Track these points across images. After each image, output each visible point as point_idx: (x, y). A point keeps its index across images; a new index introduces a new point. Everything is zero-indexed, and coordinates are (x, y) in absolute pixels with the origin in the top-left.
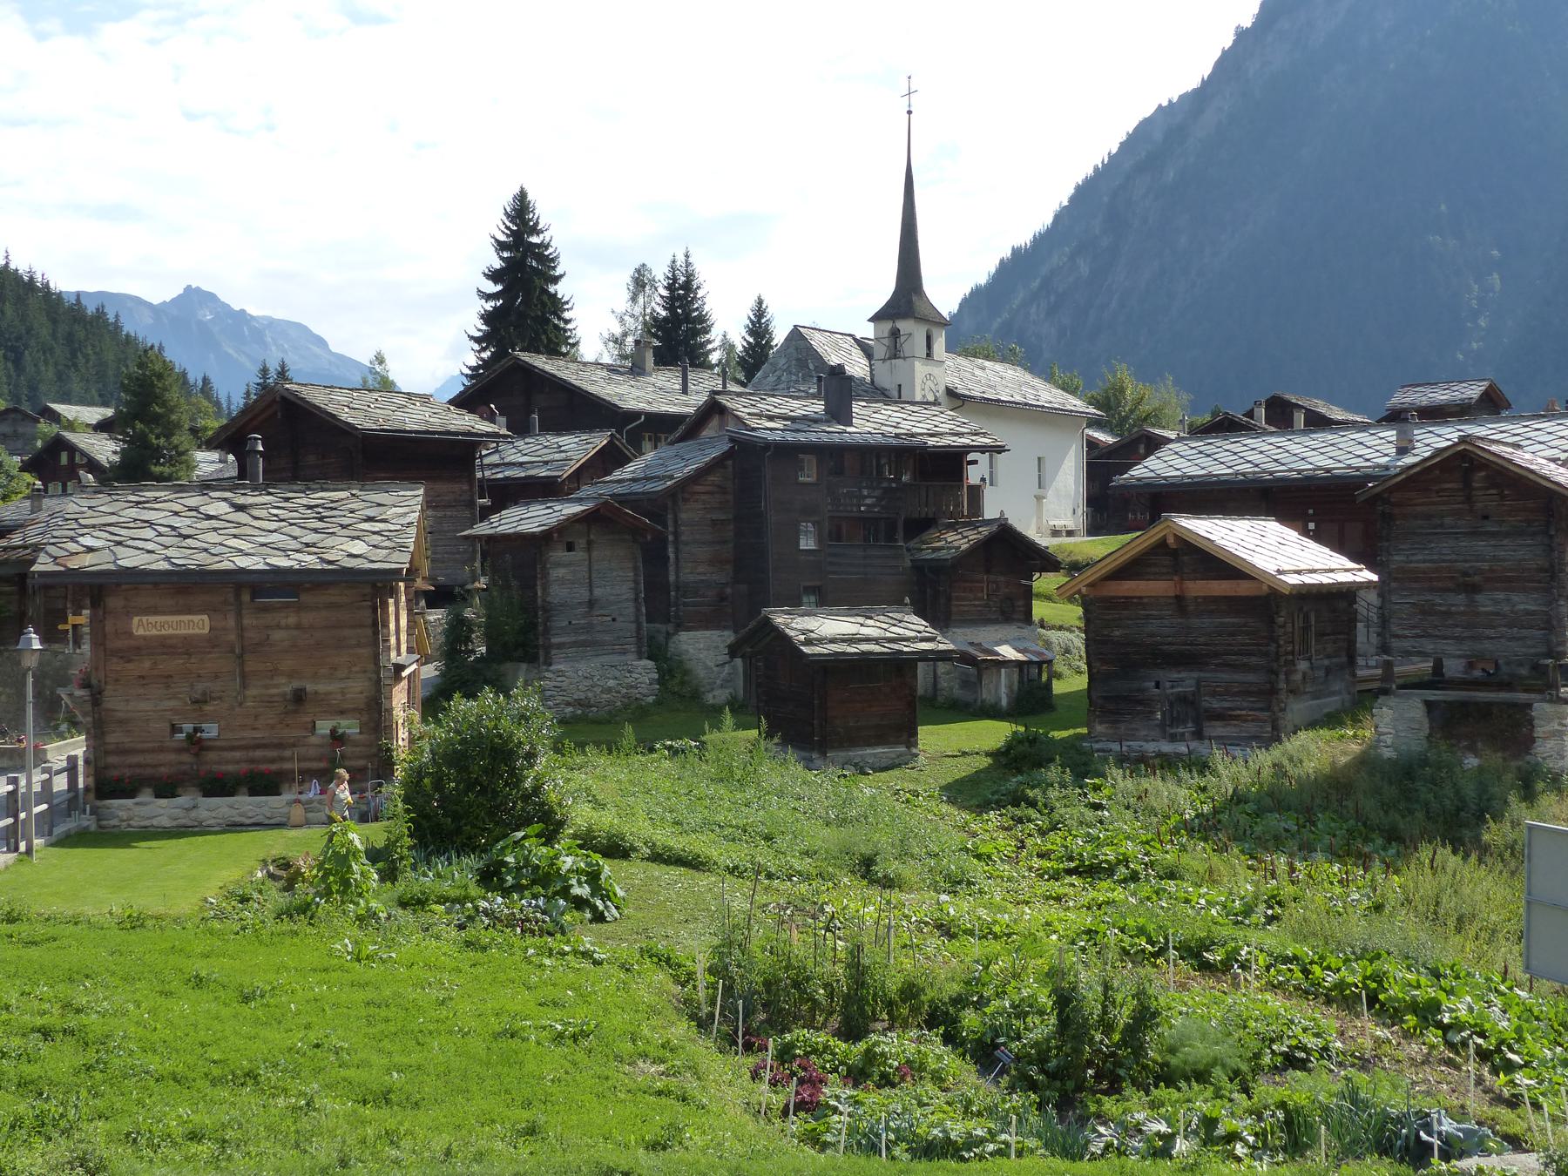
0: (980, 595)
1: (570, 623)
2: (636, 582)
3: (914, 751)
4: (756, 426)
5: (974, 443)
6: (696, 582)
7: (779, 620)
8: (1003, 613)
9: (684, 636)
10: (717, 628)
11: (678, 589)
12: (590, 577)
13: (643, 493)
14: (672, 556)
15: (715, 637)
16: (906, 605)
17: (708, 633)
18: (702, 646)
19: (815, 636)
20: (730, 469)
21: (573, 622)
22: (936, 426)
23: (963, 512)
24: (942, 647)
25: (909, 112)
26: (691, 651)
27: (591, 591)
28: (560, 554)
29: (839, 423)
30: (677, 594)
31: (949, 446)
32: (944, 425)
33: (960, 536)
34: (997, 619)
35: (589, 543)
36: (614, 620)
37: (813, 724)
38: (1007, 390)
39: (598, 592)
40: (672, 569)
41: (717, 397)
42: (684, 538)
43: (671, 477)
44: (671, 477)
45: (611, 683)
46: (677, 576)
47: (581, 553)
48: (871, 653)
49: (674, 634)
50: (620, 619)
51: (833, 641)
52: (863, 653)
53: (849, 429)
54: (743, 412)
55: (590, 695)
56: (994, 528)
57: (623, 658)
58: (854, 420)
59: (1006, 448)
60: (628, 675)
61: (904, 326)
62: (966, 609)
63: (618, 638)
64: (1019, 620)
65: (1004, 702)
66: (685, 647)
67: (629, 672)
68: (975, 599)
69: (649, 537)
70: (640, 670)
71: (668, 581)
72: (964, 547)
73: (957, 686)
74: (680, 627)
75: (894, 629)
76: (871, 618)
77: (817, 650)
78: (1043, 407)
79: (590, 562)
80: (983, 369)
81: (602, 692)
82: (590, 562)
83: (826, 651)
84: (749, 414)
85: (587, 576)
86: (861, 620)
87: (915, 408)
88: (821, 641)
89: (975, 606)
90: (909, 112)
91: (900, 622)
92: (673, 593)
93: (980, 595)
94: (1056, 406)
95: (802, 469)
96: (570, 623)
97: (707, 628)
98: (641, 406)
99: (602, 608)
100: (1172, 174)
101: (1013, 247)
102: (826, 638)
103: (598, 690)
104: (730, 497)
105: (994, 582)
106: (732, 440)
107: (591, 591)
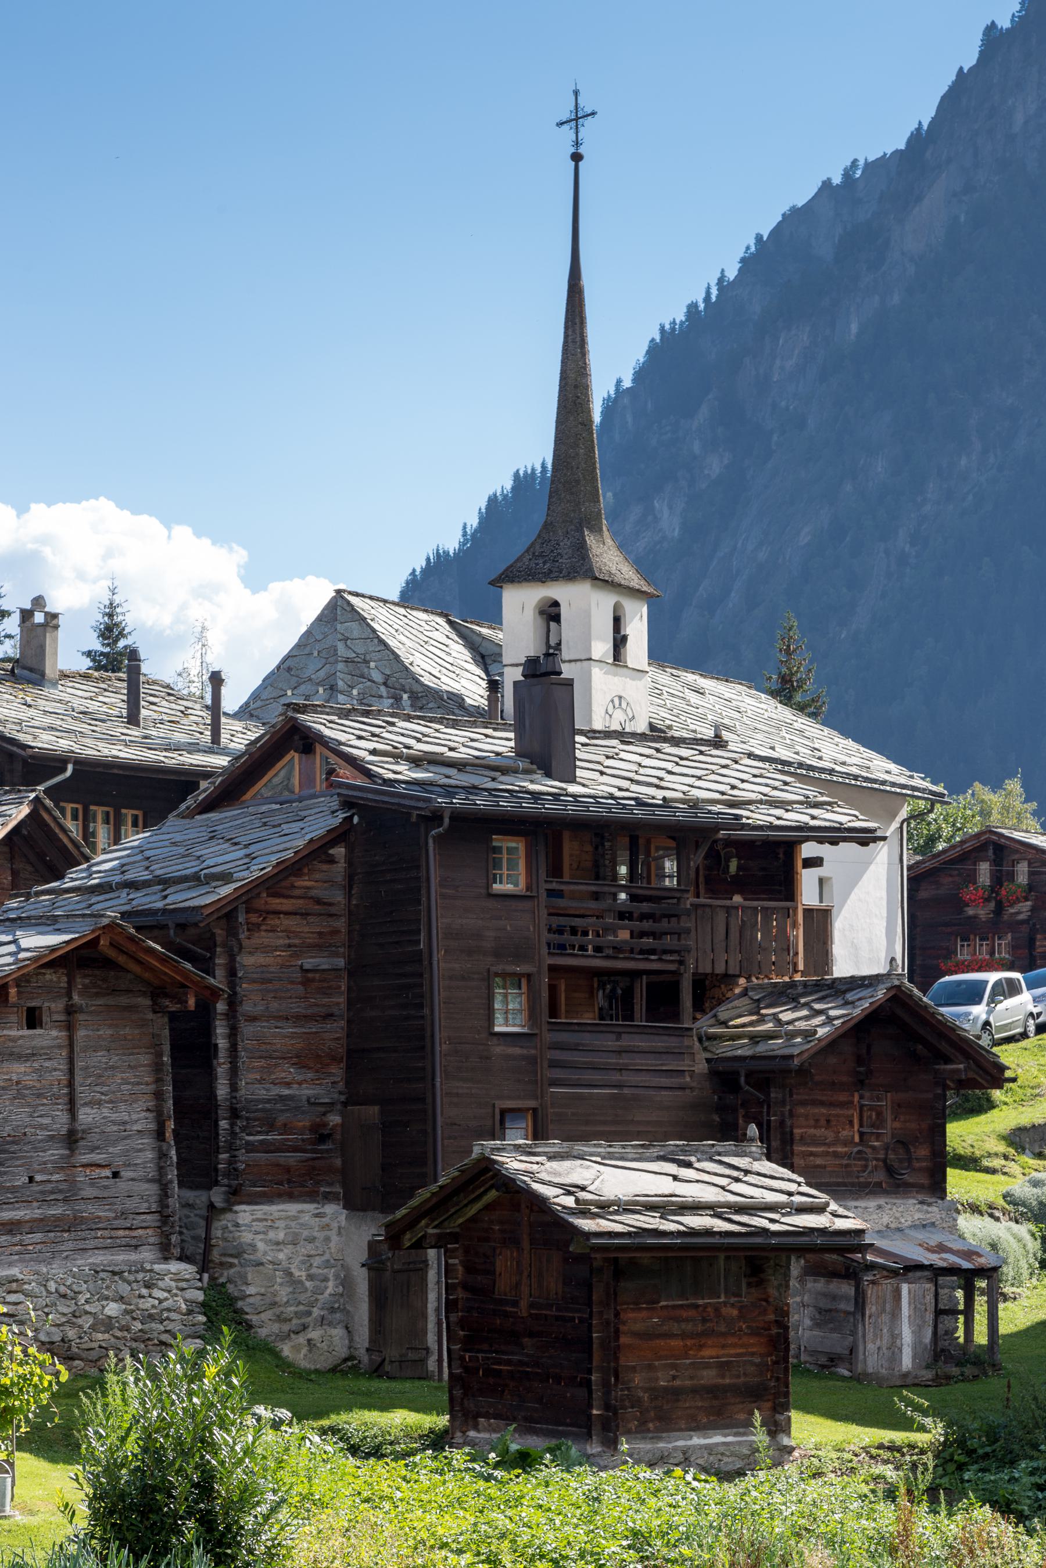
0: (845, 1133)
1: (31, 1179)
2: (158, 1095)
3: (786, 1441)
4: (392, 776)
5: (813, 823)
6: (268, 1101)
7: (516, 1165)
8: (890, 1171)
9: (245, 1213)
10: (311, 1196)
11: (234, 1114)
12: (71, 1085)
13: (164, 911)
14: (222, 1043)
15: (306, 1218)
16: (752, 1140)
17: (292, 1208)
18: (281, 1236)
19: (589, 1196)
20: (341, 866)
21: (38, 1178)
22: (733, 787)
23: (795, 965)
24: (841, 1224)
25: (577, 157)
26: (261, 1246)
27: (72, 1110)
28: (14, 1033)
29: (549, 775)
30: (232, 1125)
31: (772, 827)
32: (745, 786)
33: (805, 1012)
34: (879, 1184)
35: (70, 1011)
36: (116, 1175)
37: (588, 1383)
38: (759, 736)
39: (86, 1116)
40: (222, 1070)
41: (302, 717)
42: (247, 1007)
43: (225, 878)
44: (225, 878)
45: (113, 1309)
46: (234, 1087)
47: (54, 1033)
48: (708, 1232)
49: (224, 1210)
50: (126, 1174)
51: (628, 1207)
52: (693, 1233)
53: (573, 789)
54: (361, 749)
55: (71, 1334)
56: (880, 993)
57: (133, 1257)
58: (579, 773)
59: (879, 834)
60: (144, 1292)
61: (566, 593)
62: (819, 1161)
63: (124, 1214)
64: (920, 1188)
65: (907, 1362)
66: (247, 1237)
67: (148, 1286)
68: (837, 1141)
69: (192, 1002)
70: (168, 1282)
71: (212, 1096)
72: (821, 1032)
73: (808, 1322)
74: (236, 1195)
75: (736, 1187)
76: (689, 1165)
77: (604, 1225)
78: (831, 772)
79: (71, 1051)
80: (700, 692)
81: (93, 1327)
82: (71, 1051)
83: (619, 1228)
84: (374, 752)
85: (64, 1078)
86: (671, 1168)
87: (684, 752)
88: (605, 1208)
89: (836, 1155)
90: (577, 157)
91: (747, 1172)
92: (223, 1124)
93: (845, 1133)
94: (854, 770)
95: (497, 865)
96: (31, 1179)
97: (290, 1197)
98: (64, 744)
99: (93, 1149)
100: (854, 328)
101: (516, 474)
102: (617, 1202)
103: (87, 1322)
104: (341, 924)
105: (871, 1108)
106: (348, 804)
107: (72, 1110)
